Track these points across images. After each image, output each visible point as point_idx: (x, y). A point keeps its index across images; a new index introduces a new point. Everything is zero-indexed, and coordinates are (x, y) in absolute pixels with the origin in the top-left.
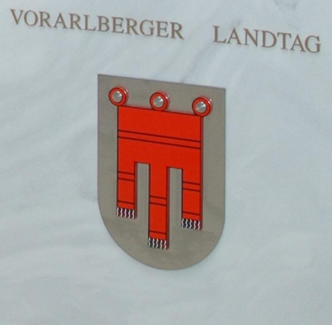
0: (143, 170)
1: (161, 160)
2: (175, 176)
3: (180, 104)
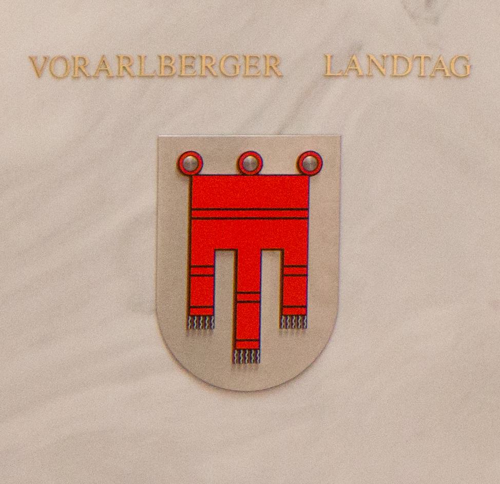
0: (225, 267)
1: (247, 233)
2: (271, 266)
3: (279, 164)
